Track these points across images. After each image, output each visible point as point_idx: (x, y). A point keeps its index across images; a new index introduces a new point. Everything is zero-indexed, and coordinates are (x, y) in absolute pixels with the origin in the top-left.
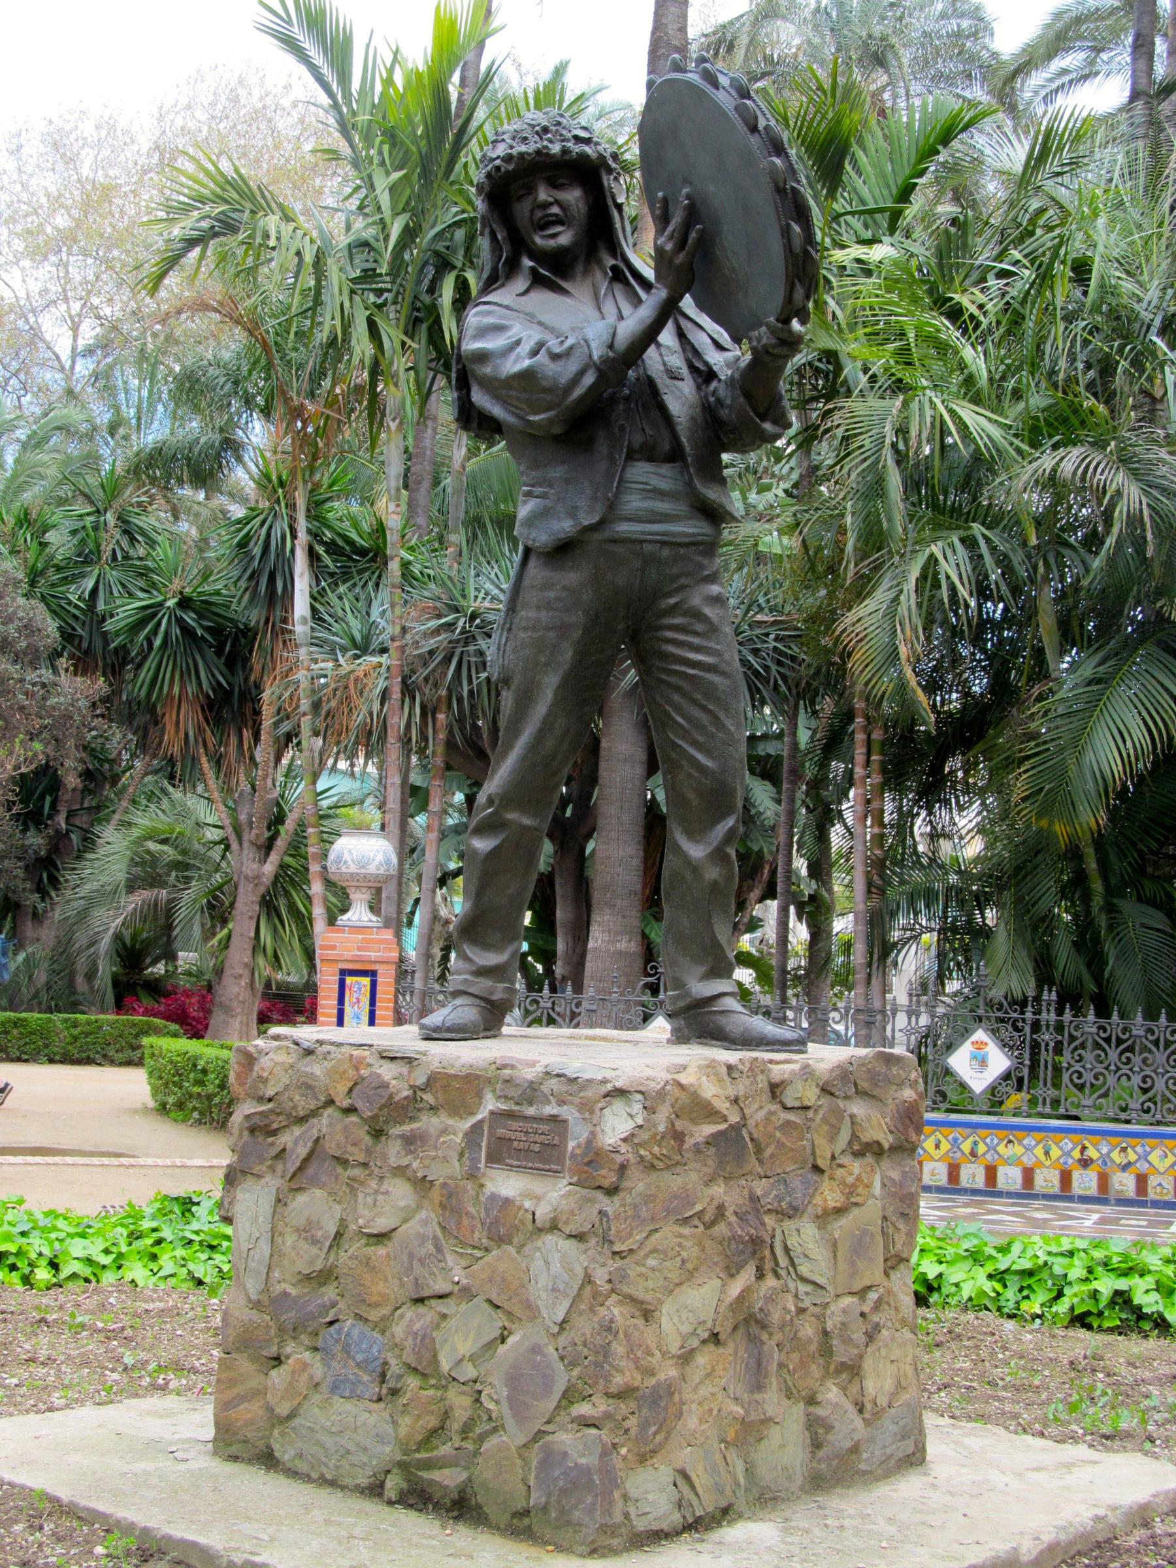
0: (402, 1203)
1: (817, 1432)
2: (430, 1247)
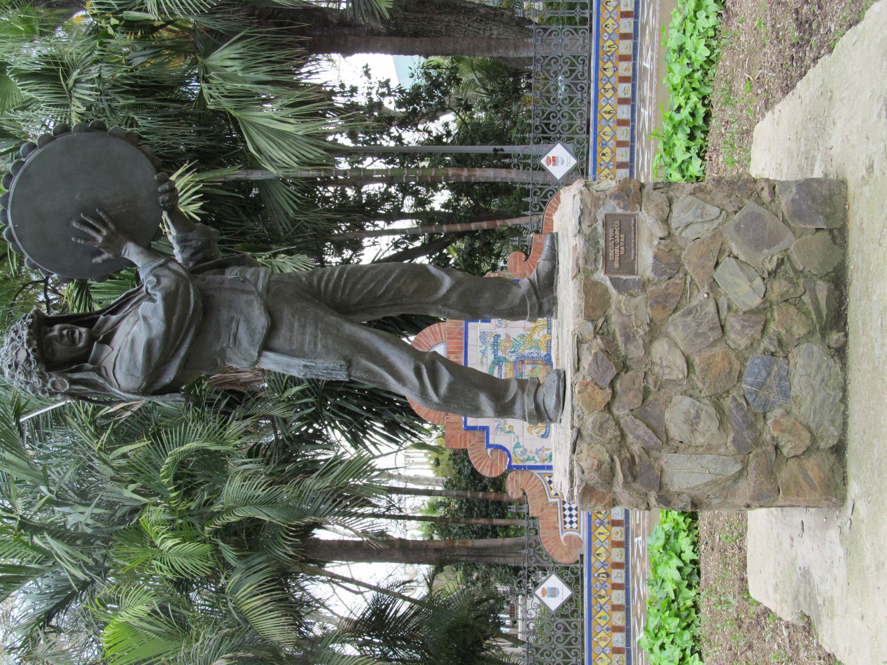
0: (666, 347)
2: (689, 319)
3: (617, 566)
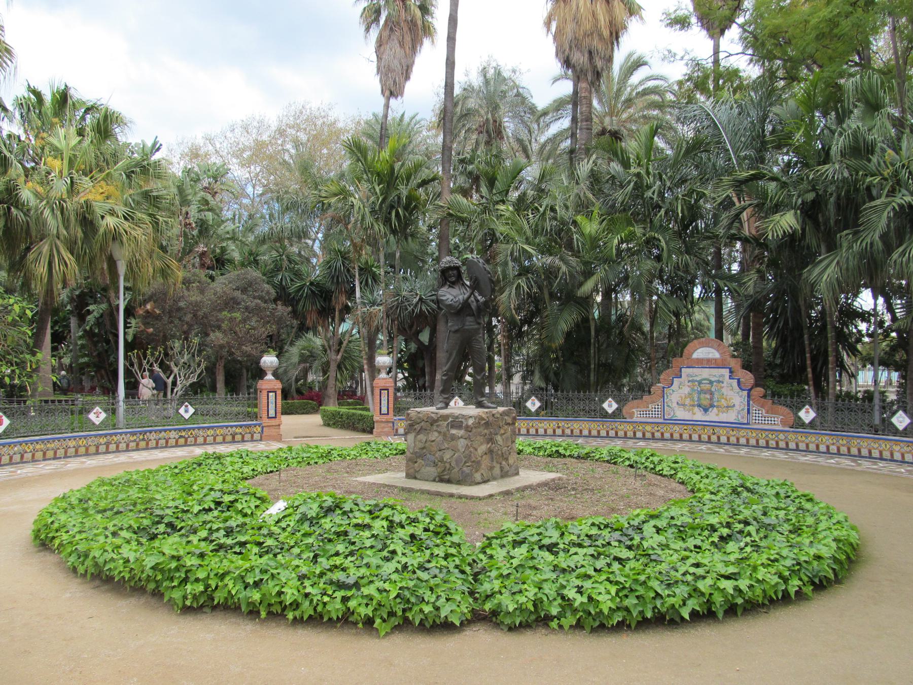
1: (502, 469)
3: (616, 433)
